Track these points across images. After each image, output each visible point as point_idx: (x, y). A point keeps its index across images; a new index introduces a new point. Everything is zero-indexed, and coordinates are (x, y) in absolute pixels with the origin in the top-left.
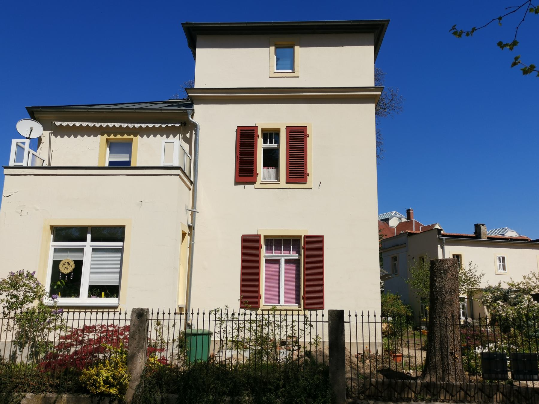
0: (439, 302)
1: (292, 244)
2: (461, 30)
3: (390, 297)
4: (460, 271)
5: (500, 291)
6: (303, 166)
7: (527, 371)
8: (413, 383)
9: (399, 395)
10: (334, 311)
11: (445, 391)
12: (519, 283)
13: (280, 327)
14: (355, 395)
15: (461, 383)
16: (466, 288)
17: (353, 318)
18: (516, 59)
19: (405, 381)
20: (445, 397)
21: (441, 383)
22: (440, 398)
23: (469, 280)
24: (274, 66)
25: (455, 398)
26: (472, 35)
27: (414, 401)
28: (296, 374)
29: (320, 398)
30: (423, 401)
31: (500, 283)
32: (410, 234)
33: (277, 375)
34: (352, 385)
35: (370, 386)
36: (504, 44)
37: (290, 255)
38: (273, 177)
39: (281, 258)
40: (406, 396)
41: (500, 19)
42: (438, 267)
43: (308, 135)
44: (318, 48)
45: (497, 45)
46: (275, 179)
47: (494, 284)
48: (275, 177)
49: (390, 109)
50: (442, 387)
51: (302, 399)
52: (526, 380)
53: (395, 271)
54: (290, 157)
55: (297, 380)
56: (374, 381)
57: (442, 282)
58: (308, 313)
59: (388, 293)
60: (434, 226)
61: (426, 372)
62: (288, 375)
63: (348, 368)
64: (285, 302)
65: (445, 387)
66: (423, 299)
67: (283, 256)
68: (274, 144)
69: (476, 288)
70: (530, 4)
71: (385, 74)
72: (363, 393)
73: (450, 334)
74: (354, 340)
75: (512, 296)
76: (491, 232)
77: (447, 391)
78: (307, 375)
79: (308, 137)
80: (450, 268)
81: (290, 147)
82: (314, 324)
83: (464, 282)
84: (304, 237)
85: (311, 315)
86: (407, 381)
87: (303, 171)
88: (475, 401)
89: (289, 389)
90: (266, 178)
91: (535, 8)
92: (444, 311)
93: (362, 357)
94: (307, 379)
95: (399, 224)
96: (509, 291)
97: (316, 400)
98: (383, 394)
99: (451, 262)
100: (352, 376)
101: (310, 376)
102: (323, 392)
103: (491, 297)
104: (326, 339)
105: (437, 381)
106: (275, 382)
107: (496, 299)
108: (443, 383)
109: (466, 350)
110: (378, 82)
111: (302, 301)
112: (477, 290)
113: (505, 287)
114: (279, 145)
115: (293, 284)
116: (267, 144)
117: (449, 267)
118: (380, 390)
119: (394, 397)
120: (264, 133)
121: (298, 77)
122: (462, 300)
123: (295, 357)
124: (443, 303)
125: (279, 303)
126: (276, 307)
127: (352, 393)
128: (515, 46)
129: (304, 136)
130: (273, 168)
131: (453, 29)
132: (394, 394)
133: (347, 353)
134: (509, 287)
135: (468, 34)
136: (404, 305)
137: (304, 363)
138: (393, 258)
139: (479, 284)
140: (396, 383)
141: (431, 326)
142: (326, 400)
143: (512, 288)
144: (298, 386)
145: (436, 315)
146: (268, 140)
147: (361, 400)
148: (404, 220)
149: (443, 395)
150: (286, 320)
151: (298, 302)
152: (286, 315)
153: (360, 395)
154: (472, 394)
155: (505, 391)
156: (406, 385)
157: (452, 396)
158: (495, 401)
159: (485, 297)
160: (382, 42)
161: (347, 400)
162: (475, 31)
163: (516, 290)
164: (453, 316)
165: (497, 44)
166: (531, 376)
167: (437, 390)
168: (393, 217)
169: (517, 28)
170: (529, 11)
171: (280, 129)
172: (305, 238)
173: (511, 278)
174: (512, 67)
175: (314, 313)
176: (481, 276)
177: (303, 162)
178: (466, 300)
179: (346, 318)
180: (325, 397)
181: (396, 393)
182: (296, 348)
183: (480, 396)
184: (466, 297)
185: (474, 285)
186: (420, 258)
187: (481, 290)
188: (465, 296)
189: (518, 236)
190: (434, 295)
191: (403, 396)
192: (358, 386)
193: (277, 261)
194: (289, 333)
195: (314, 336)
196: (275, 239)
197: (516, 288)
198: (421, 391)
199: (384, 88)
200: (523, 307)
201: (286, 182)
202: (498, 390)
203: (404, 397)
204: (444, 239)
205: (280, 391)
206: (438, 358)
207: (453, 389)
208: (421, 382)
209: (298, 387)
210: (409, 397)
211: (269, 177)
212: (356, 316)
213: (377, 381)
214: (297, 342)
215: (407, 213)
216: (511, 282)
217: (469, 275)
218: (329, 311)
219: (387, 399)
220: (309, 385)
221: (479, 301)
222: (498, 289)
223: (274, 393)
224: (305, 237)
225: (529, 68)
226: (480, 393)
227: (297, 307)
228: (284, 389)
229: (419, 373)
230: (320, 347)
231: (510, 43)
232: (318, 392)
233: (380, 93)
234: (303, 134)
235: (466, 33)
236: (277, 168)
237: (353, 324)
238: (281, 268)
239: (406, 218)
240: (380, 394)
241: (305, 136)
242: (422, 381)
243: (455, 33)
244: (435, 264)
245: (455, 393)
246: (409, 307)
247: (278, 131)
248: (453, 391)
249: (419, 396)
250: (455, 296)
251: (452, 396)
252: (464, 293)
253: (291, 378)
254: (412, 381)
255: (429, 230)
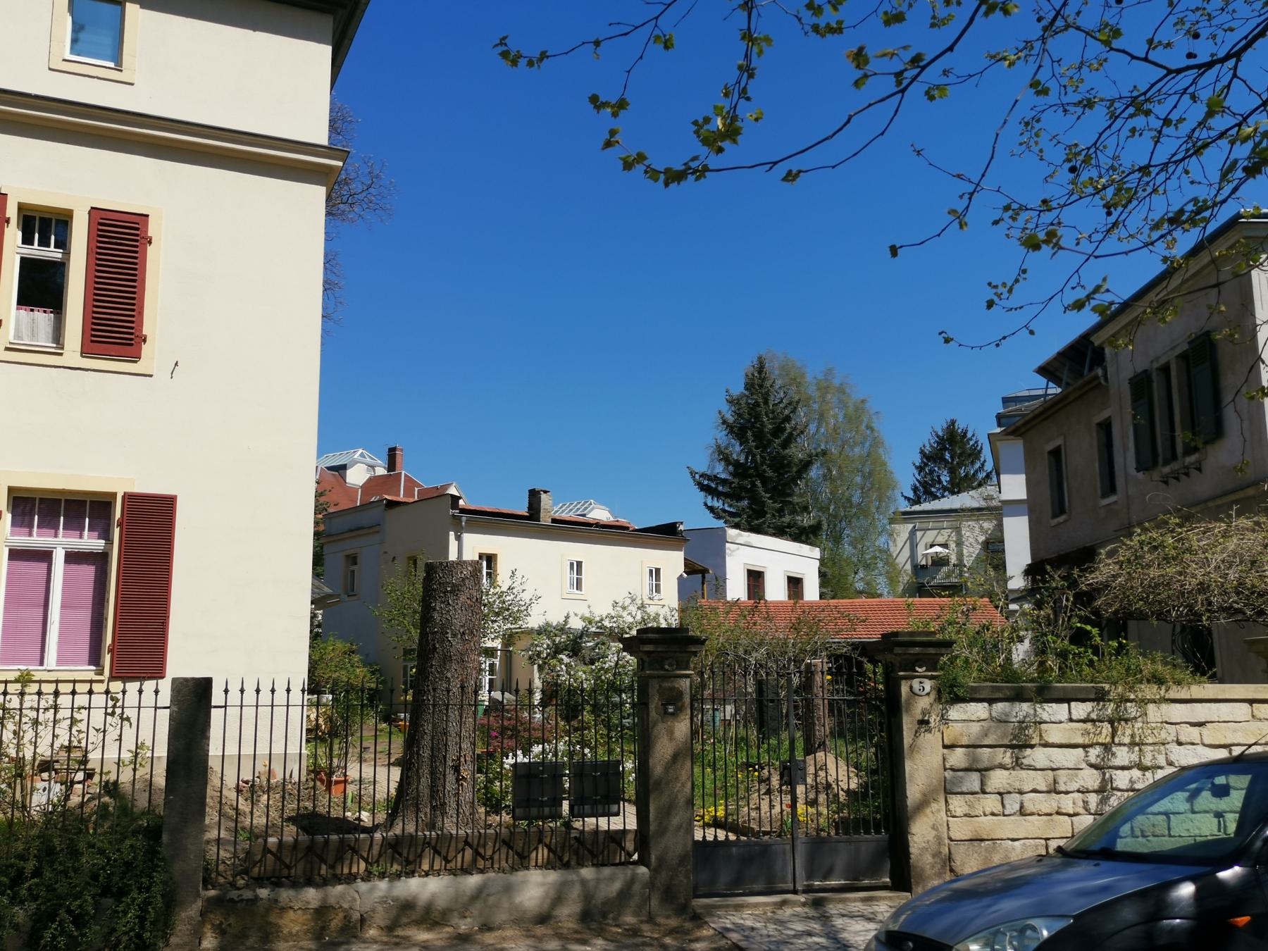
0: (436, 656)
1: (64, 511)
2: (518, 52)
3: (333, 649)
4: (492, 590)
5: (567, 633)
6: (133, 316)
7: (599, 797)
8: (364, 840)
9: (329, 871)
10: (186, 680)
11: (432, 851)
12: (604, 616)
13: (36, 722)
14: (226, 878)
15: (468, 831)
16: (500, 627)
17: (234, 697)
18: (613, 133)
19: (346, 836)
20: (432, 866)
21: (425, 835)
22: (420, 868)
23: (508, 610)
24: (64, 42)
25: (452, 865)
26: (539, 66)
27: (363, 880)
28: (72, 840)
29: (135, 894)
30: (384, 878)
31: (567, 617)
32: (392, 504)
33: (20, 846)
34: (220, 856)
35: (264, 856)
36: (602, 102)
37: (80, 540)
38: (44, 336)
39: (55, 548)
40: (346, 871)
41: (597, 43)
42: (440, 578)
43: (151, 240)
44: (189, 20)
45: (588, 100)
46: (50, 340)
47: (556, 619)
48: (51, 336)
49: (365, 206)
50: (428, 843)
51: (86, 901)
52: (596, 816)
53: (350, 589)
54: (96, 289)
55: (74, 853)
56: (274, 843)
57: (448, 611)
58: (116, 686)
59: (331, 639)
60: (447, 489)
61: (397, 813)
62: (52, 844)
63: (211, 816)
64: (59, 662)
65: (433, 843)
66: (407, 652)
67: (61, 542)
68: (52, 248)
69: (520, 628)
70: (656, 26)
71: (358, 122)
72: (246, 872)
73: (453, 727)
74: (232, 750)
75: (589, 644)
76: (561, 507)
77: (437, 852)
78: (103, 842)
79: (150, 242)
80: (467, 581)
81: (98, 262)
82: (131, 713)
83: (497, 614)
84: (124, 497)
85: (124, 692)
86: (351, 836)
87: (132, 328)
88: (493, 868)
89: (50, 879)
90: (25, 337)
91: (665, 36)
92: (446, 677)
93: (251, 790)
94: (101, 852)
95: (370, 480)
96: (584, 633)
97: (123, 900)
98: (293, 871)
99: (469, 568)
100: (222, 836)
101: (110, 843)
102: (144, 880)
103: (548, 645)
104: (162, 751)
105: (416, 831)
106: (12, 866)
107: (557, 650)
108: (431, 835)
109: (483, 762)
110: (341, 137)
111: (107, 659)
112: (522, 632)
113: (576, 624)
114: (67, 253)
115: (84, 617)
116: (33, 245)
117: (463, 580)
118: (287, 861)
119: (319, 874)
120: (24, 216)
121: (132, 84)
122: (490, 652)
123: (75, 800)
124: (447, 659)
125: (42, 664)
126: (32, 673)
127: (219, 874)
128: (622, 111)
129: (138, 238)
130: (45, 312)
131: (501, 44)
132: (320, 869)
133: (214, 781)
134: (584, 624)
135: (531, 64)
136: (364, 666)
137: (96, 813)
138: (347, 556)
139: (528, 618)
140: (327, 842)
141: (417, 710)
142: (148, 897)
143: (590, 626)
144: (75, 871)
145: (428, 686)
146: (37, 236)
147: (239, 889)
148: (381, 471)
149: (428, 861)
150: (56, 708)
151: (95, 659)
152: (56, 694)
153: (238, 877)
154: (489, 853)
155: (554, 841)
156: (349, 846)
157: (447, 861)
158: (534, 864)
159: (537, 645)
160: (352, 40)
161: (203, 893)
162: (545, 59)
163: (598, 630)
164: (462, 687)
165: (589, 98)
166: (607, 806)
167: (416, 851)
168: (357, 462)
169: (629, 72)
170: (652, 40)
171: (71, 211)
172: (126, 500)
173: (589, 607)
174: (603, 149)
175: (133, 687)
176: (533, 601)
177: (134, 305)
178: (499, 652)
179: (217, 697)
180: (148, 889)
181: (324, 867)
182: (80, 776)
183: (503, 856)
184: (499, 648)
185: (516, 620)
186: (410, 558)
187: (530, 632)
188: (497, 644)
189: (612, 519)
190: (427, 641)
191: (338, 871)
192: (235, 855)
193: (45, 556)
194: (63, 740)
195: (129, 743)
196: (66, 500)
197: (597, 628)
198: (380, 855)
199: (349, 152)
200: (606, 666)
201: (82, 353)
202: (540, 841)
203: (342, 874)
204: (464, 519)
205: (26, 885)
206: (425, 781)
207: (449, 846)
208: (383, 836)
209: (75, 874)
210: (352, 872)
211: (33, 335)
212: (242, 691)
213: (280, 841)
214: (84, 761)
215: (389, 455)
216: (587, 615)
217: (508, 598)
218: (174, 680)
219: (301, 880)
220: (107, 865)
221: (523, 656)
222: (562, 629)
223: (9, 892)
224: (126, 497)
225: (635, 159)
226: (504, 850)
227: (93, 673)
228: (36, 880)
229: (381, 817)
230: (143, 772)
231: (613, 102)
232: (129, 880)
233: (340, 164)
234: (137, 235)
235: (528, 59)
236: (58, 313)
237: (233, 712)
238: (52, 575)
239: (385, 468)
240: (285, 872)
241: (143, 241)
242: (385, 835)
243: (505, 55)
244: (435, 572)
245: (454, 854)
246: (376, 670)
247: (65, 215)
248: (450, 850)
249: (375, 869)
250: (472, 644)
251: (447, 861)
252: (496, 637)
253: (60, 851)
254: (362, 836)
255: (437, 496)
